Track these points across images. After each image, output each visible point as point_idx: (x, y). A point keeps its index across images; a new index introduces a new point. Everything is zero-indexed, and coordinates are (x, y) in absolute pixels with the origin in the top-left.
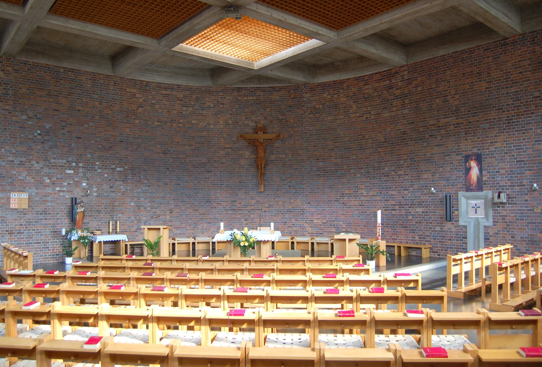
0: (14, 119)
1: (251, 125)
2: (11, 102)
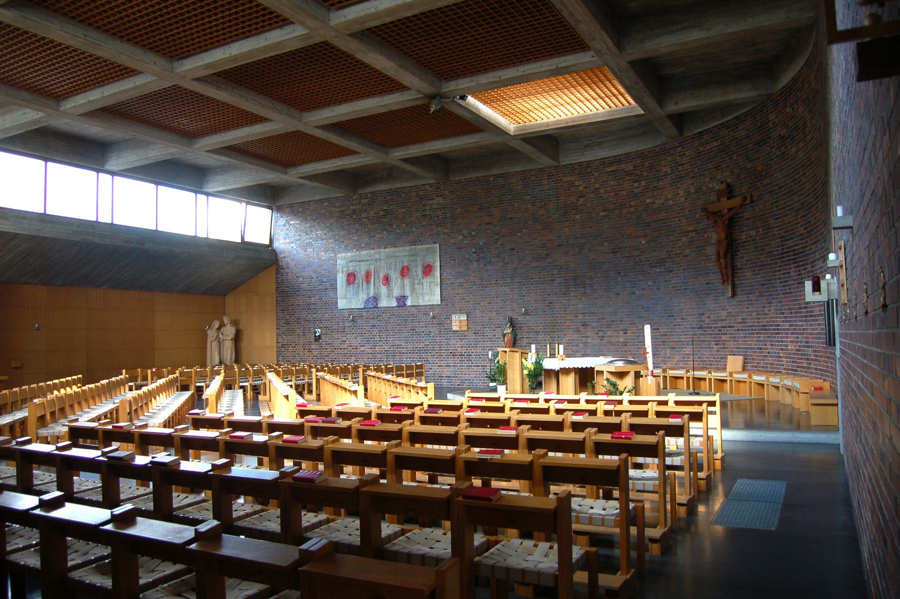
0: (452, 241)
1: (716, 188)
2: (449, 225)
